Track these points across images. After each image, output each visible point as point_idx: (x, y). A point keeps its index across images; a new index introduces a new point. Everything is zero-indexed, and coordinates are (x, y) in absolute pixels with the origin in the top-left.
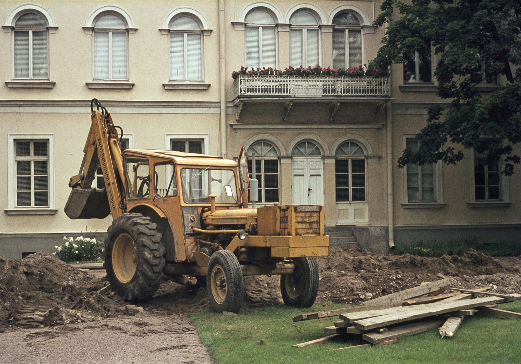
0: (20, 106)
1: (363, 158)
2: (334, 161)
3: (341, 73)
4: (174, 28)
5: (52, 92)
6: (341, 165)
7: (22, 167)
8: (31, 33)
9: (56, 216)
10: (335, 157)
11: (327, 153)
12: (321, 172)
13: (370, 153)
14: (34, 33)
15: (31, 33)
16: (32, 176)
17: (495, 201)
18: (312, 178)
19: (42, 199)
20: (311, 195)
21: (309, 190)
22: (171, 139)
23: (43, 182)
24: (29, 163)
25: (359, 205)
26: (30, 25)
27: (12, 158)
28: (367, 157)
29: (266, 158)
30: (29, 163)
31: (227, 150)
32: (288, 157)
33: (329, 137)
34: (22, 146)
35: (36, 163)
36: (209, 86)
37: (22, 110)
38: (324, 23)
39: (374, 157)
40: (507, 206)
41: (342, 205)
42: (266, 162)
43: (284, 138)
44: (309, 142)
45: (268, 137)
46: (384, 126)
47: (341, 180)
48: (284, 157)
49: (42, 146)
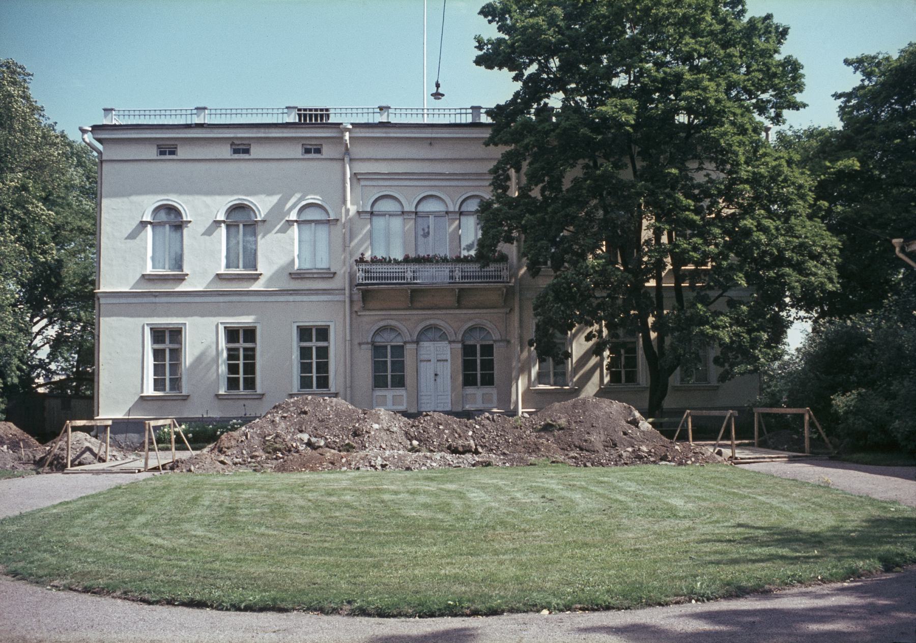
0: (156, 296)
1: (491, 342)
2: (460, 345)
3: (459, 260)
4: (303, 218)
5: (184, 283)
6: (468, 350)
7: (305, 353)
8: (241, 226)
9: (264, 399)
10: (463, 342)
11: (453, 338)
12: (449, 357)
13: (408, 339)
14: (244, 225)
15: (241, 226)
16: (389, 359)
17: (631, 385)
18: (439, 363)
19: (323, 382)
20: (438, 380)
21: (436, 375)
22: (298, 327)
23: (323, 367)
24: (311, 348)
25: (487, 390)
26: (238, 216)
27: (295, 344)
28: (405, 343)
29: (484, 343)
30: (311, 348)
31: (351, 335)
32: (413, 342)
33: (455, 322)
34: (304, 333)
35: (317, 348)
36: (335, 273)
37: (157, 300)
38: (451, 209)
39: (501, 341)
40: (186, 398)
41: (470, 390)
42: (392, 347)
43: (408, 323)
44: (435, 328)
45: (393, 323)
46: (511, 310)
47: (468, 365)
48: (409, 342)
49: (250, 334)
